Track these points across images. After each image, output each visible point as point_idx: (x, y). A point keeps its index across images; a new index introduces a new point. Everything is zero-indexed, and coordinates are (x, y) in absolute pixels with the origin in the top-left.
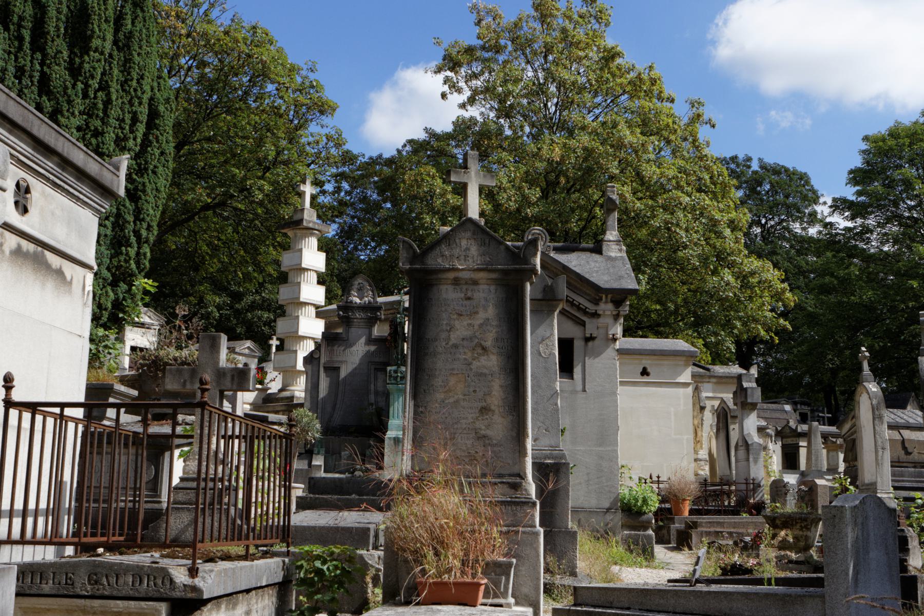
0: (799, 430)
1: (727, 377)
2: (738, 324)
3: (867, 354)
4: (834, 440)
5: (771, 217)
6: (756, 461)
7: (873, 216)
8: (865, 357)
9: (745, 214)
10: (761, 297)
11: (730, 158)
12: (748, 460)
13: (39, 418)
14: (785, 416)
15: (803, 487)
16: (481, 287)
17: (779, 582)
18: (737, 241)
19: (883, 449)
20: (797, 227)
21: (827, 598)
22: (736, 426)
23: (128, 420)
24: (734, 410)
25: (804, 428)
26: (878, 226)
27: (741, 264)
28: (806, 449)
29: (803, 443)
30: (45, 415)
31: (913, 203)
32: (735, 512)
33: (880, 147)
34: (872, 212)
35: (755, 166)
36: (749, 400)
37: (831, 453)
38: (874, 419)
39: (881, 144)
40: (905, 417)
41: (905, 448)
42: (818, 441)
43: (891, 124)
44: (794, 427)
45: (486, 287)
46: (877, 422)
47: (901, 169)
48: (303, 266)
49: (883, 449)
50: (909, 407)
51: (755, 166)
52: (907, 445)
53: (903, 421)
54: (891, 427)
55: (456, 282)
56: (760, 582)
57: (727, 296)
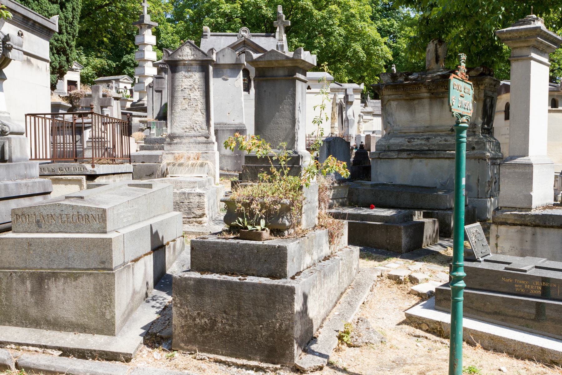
12: (348, 127)
13: (37, 118)
16: (194, 66)
23: (69, 118)
30: (39, 117)
45: (195, 66)
48: (145, 42)
55: (184, 65)
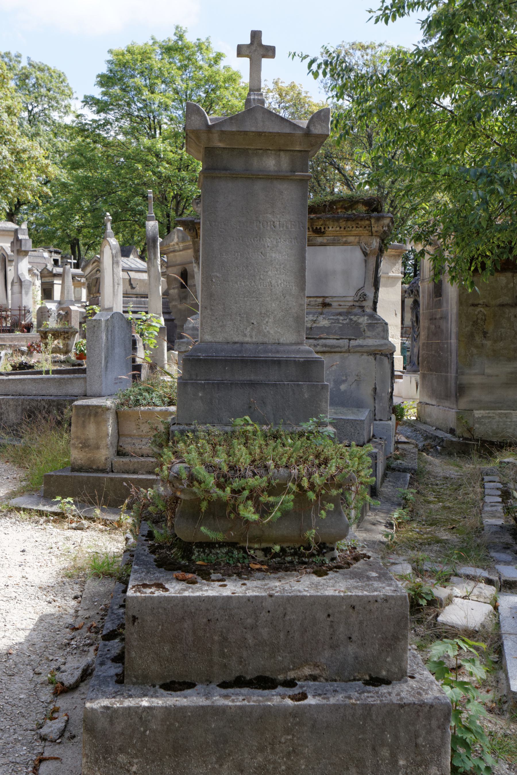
0: (54, 272)
1: (4, 231)
2: (12, 189)
3: (110, 218)
4: (79, 279)
5: (36, 105)
6: (27, 293)
7: (112, 112)
8: (109, 220)
9: (19, 103)
10: (29, 169)
11: (5, 54)
12: (21, 293)
14: (43, 261)
15: (61, 312)
17: (55, 372)
18: (12, 123)
19: (118, 284)
20: (55, 115)
21: (88, 379)
22: (12, 268)
24: (11, 255)
25: (59, 270)
26: (116, 121)
27: (15, 142)
28: (60, 286)
29: (57, 282)
31: (141, 106)
32: (10, 331)
33: (120, 60)
34: (112, 109)
35: (24, 63)
36: (23, 249)
37: (77, 289)
38: (113, 263)
39: (121, 57)
40: (129, 263)
41: (131, 284)
42: (69, 279)
43: (129, 43)
44: (51, 270)
46: (115, 266)
47: (134, 78)
49: (118, 284)
50: (131, 256)
51: (24, 63)
52: (132, 282)
53: (127, 266)
54: (123, 270)
56: (40, 373)
57: (4, 168)
